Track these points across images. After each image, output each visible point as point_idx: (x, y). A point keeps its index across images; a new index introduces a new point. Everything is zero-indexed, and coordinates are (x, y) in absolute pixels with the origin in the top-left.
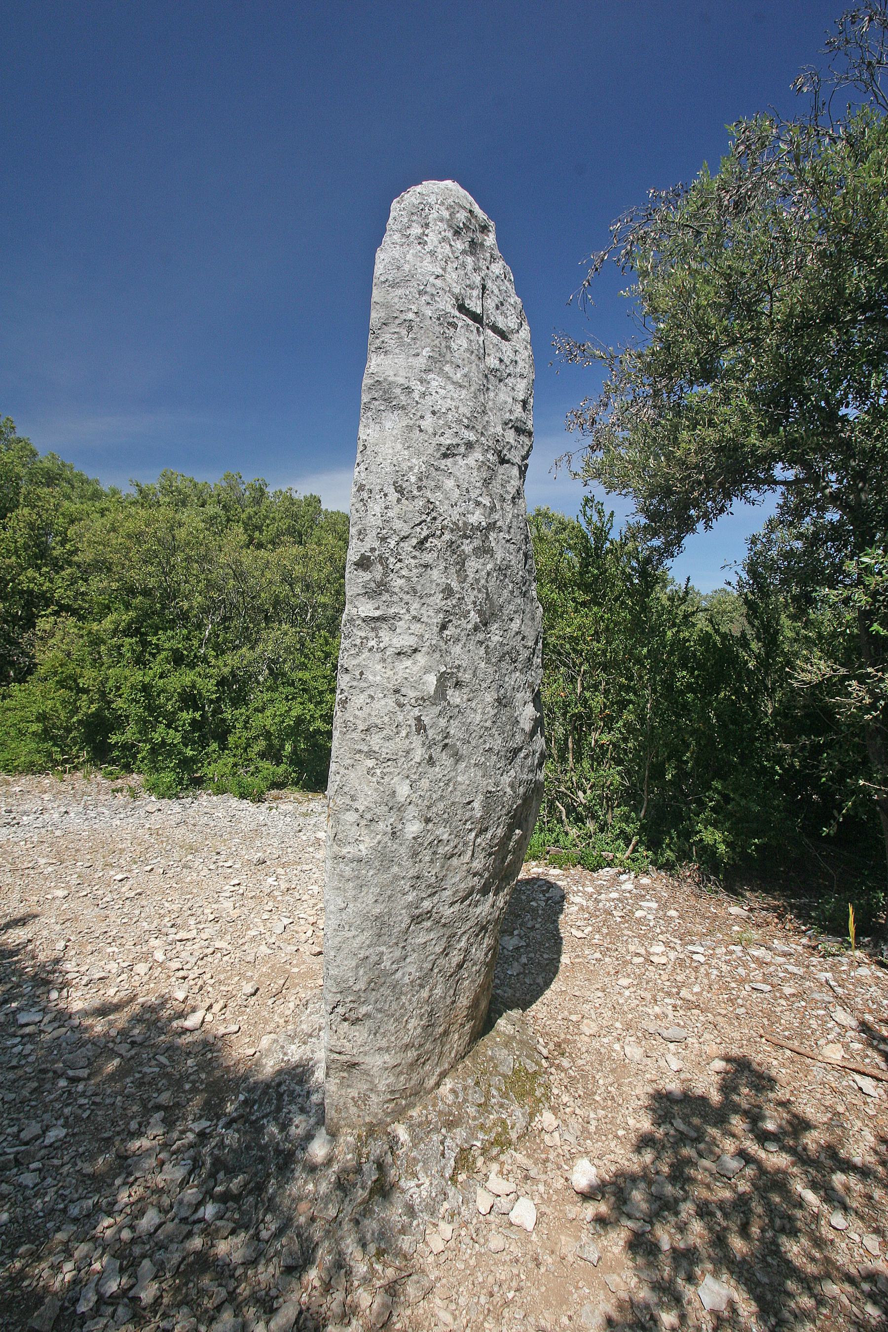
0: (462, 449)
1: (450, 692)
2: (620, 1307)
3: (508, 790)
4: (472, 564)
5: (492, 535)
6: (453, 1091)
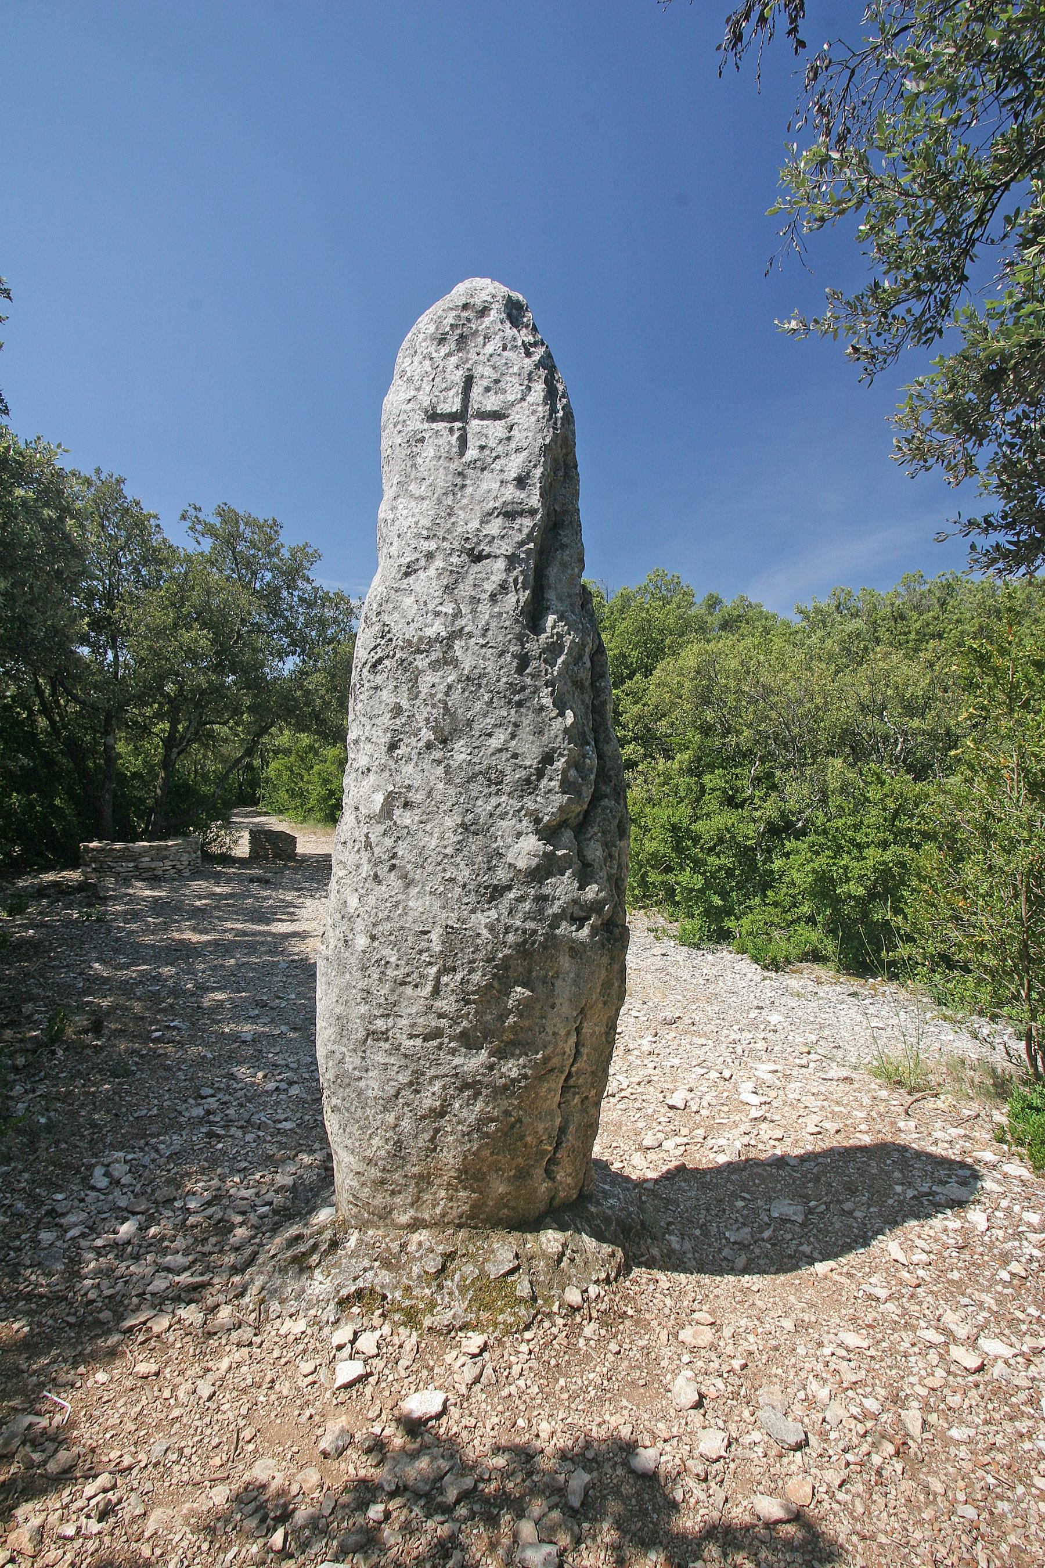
0: (422, 563)
1: (397, 812)
2: (282, 1492)
3: (485, 932)
4: (428, 679)
5: (458, 644)
6: (420, 1244)
